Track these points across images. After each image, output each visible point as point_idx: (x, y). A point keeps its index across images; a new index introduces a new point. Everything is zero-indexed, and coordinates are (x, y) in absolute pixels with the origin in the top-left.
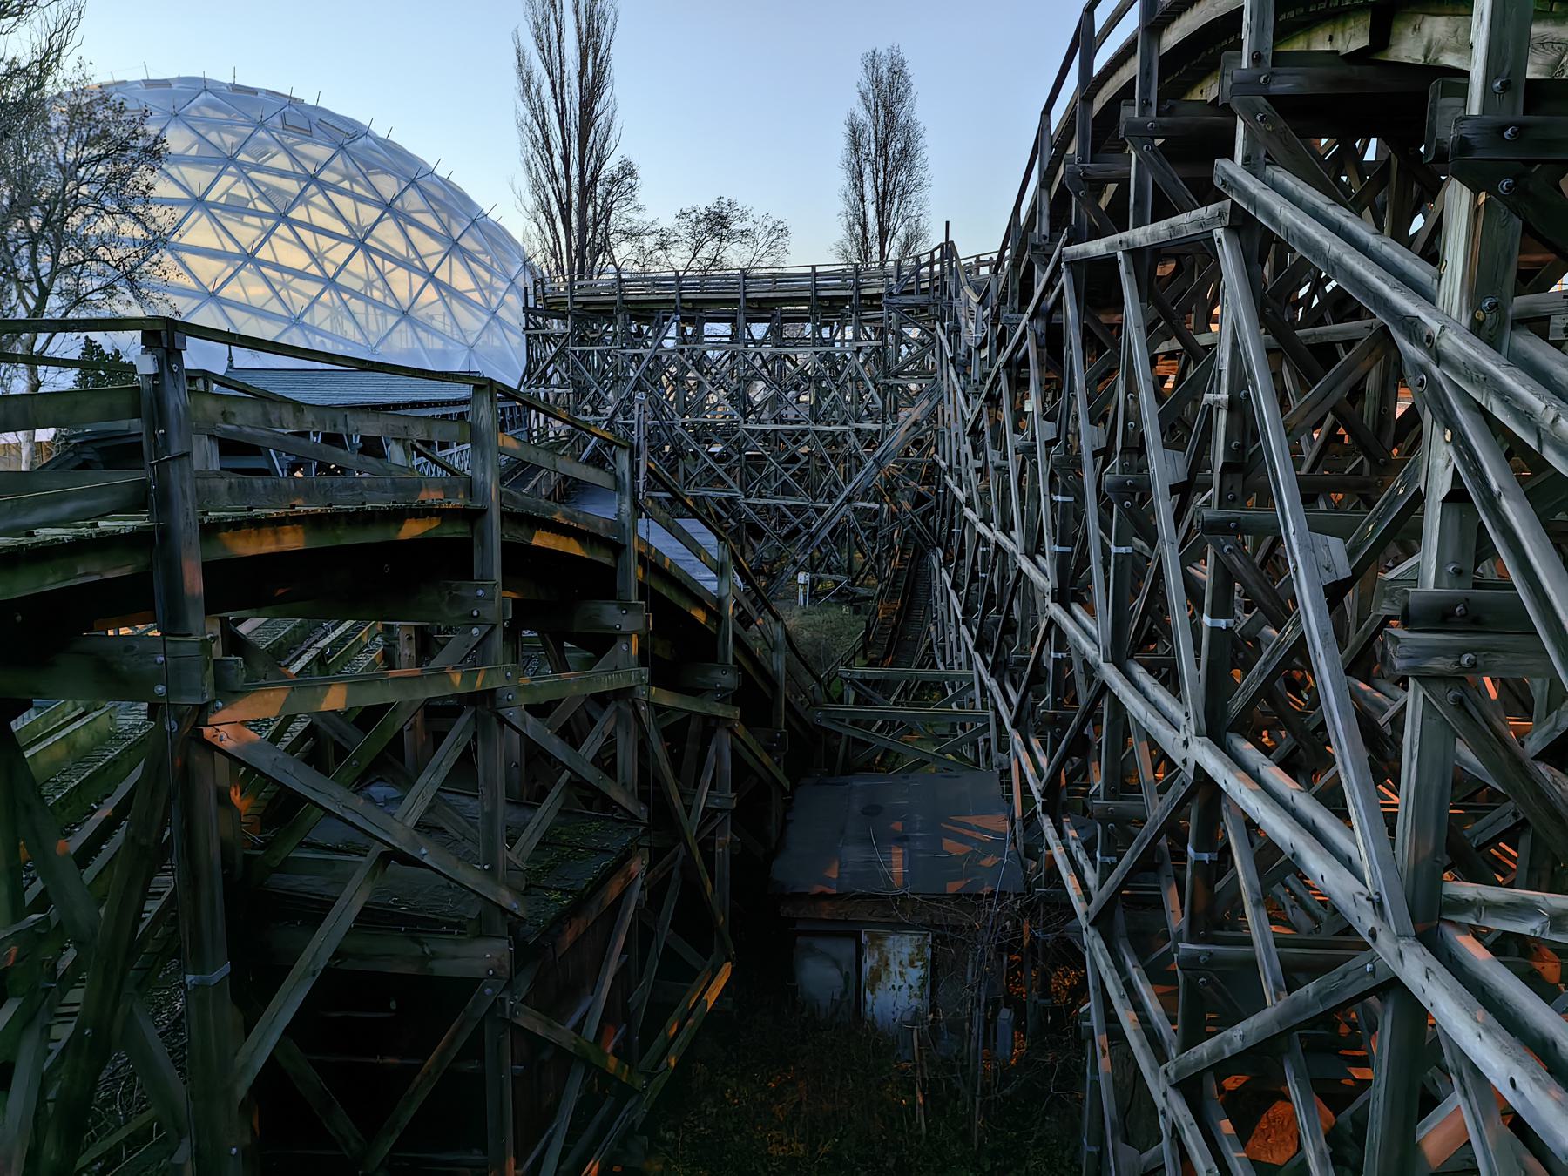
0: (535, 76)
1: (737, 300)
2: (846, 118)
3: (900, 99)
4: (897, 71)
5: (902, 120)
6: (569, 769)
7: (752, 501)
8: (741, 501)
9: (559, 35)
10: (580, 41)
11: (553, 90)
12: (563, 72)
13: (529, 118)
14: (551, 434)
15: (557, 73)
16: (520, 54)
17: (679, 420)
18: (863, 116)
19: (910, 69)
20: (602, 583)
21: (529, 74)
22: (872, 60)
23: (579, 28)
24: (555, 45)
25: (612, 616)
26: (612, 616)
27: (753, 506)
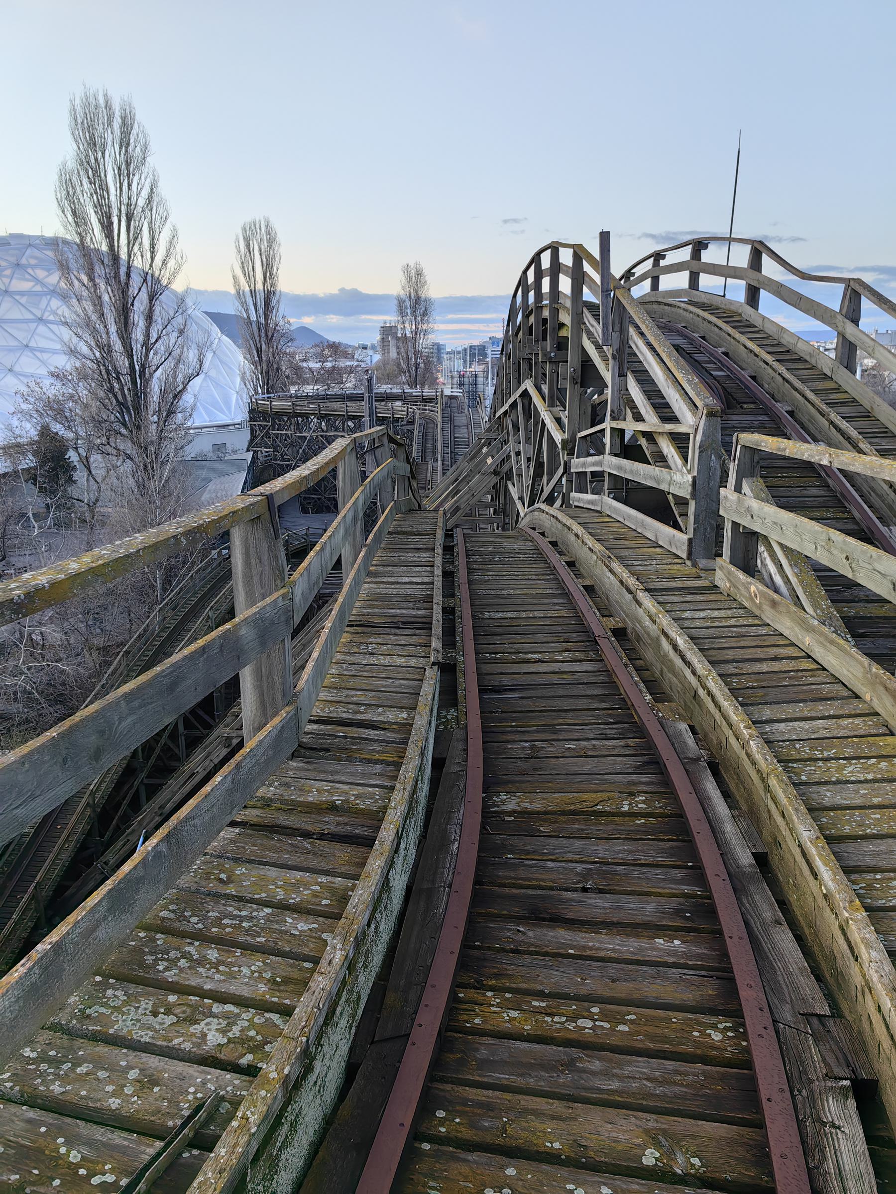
4: (419, 274)
13: (240, 308)
19: (425, 272)
24: (251, 273)
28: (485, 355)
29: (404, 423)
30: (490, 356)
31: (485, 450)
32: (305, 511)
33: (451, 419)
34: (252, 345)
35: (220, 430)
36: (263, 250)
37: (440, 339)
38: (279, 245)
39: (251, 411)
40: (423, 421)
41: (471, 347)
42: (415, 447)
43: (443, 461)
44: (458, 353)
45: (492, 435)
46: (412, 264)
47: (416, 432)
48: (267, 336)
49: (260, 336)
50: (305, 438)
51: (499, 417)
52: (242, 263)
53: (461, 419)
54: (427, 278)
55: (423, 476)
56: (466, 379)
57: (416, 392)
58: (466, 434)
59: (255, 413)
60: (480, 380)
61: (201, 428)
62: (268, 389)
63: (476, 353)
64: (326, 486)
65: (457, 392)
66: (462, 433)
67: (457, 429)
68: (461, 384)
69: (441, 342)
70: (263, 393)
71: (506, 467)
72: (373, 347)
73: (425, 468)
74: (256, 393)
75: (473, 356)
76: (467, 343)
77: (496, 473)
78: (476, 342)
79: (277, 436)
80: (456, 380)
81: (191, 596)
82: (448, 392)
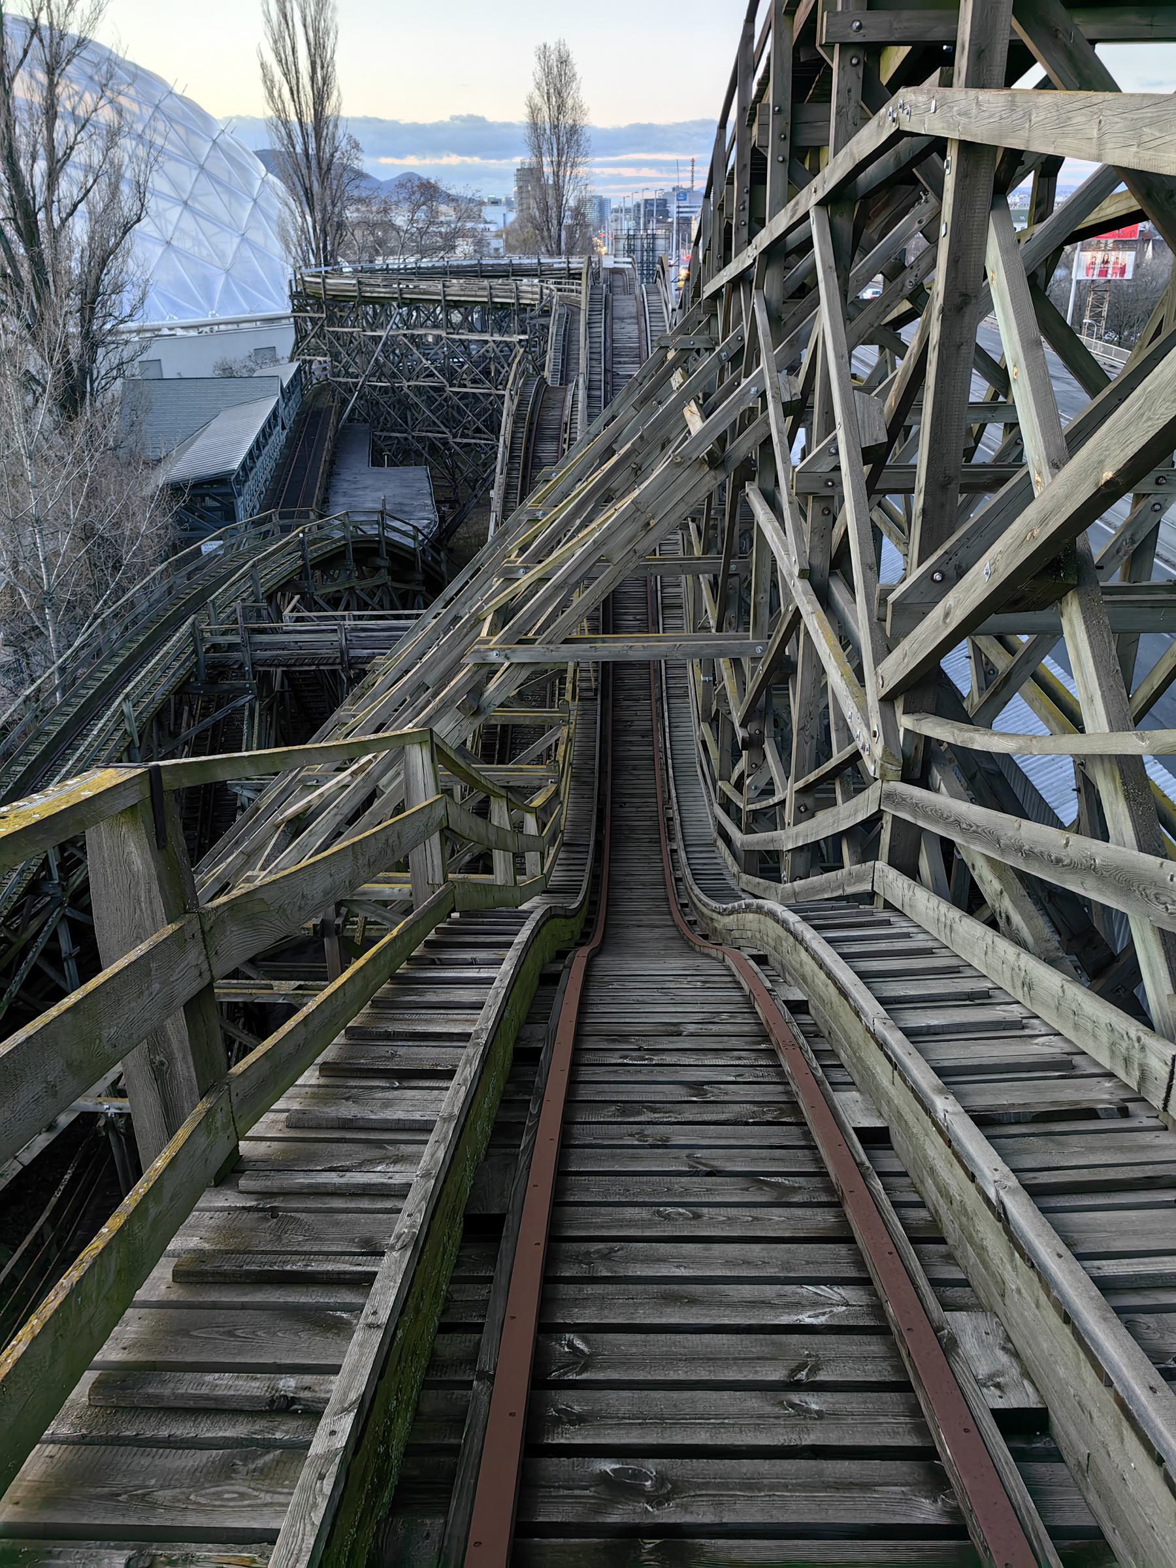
0: (276, 79)
1: (440, 301)
2: (525, 100)
3: (568, 84)
4: (564, 61)
5: (570, 102)
6: (810, 494)
7: (458, 440)
8: (451, 440)
9: (293, 49)
10: (309, 50)
11: (292, 94)
12: (298, 78)
14: (315, 381)
15: (294, 82)
16: (263, 66)
17: (406, 384)
18: (539, 100)
19: (574, 58)
20: (376, 552)
21: (272, 81)
22: (544, 52)
23: (308, 40)
24: (290, 59)
25: (380, 562)
26: (380, 562)
27: (458, 444)
28: (666, 214)
29: (537, 312)
30: (675, 215)
31: (677, 379)
32: (377, 461)
33: (608, 305)
34: (297, 183)
35: (266, 326)
36: (309, 19)
37: (597, 190)
38: (334, 9)
39: (293, 296)
40: (564, 310)
41: (646, 201)
42: (550, 354)
43: (589, 388)
44: (628, 211)
45: (695, 340)
46: (552, 45)
47: (552, 330)
48: (320, 168)
49: (309, 168)
50: (380, 337)
51: (716, 295)
52: (275, 42)
53: (626, 305)
54: (576, 68)
55: (557, 413)
56: (638, 243)
57: (559, 262)
58: (635, 333)
59: (302, 298)
60: (660, 243)
61: (238, 323)
62: (325, 257)
63: (656, 209)
64: (415, 419)
65: (624, 262)
66: (628, 332)
67: (617, 326)
68: (630, 251)
69: (605, 196)
70: (318, 265)
71: (744, 446)
72: (509, 203)
73: (560, 396)
74: (307, 265)
75: (649, 214)
76: (639, 198)
77: (715, 461)
78: (651, 195)
79: (337, 336)
80: (623, 243)
81: (103, 663)
82: (608, 262)
